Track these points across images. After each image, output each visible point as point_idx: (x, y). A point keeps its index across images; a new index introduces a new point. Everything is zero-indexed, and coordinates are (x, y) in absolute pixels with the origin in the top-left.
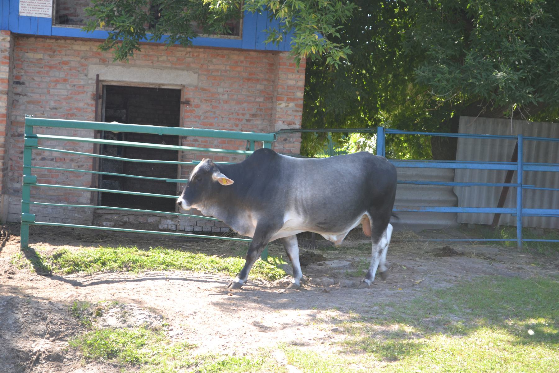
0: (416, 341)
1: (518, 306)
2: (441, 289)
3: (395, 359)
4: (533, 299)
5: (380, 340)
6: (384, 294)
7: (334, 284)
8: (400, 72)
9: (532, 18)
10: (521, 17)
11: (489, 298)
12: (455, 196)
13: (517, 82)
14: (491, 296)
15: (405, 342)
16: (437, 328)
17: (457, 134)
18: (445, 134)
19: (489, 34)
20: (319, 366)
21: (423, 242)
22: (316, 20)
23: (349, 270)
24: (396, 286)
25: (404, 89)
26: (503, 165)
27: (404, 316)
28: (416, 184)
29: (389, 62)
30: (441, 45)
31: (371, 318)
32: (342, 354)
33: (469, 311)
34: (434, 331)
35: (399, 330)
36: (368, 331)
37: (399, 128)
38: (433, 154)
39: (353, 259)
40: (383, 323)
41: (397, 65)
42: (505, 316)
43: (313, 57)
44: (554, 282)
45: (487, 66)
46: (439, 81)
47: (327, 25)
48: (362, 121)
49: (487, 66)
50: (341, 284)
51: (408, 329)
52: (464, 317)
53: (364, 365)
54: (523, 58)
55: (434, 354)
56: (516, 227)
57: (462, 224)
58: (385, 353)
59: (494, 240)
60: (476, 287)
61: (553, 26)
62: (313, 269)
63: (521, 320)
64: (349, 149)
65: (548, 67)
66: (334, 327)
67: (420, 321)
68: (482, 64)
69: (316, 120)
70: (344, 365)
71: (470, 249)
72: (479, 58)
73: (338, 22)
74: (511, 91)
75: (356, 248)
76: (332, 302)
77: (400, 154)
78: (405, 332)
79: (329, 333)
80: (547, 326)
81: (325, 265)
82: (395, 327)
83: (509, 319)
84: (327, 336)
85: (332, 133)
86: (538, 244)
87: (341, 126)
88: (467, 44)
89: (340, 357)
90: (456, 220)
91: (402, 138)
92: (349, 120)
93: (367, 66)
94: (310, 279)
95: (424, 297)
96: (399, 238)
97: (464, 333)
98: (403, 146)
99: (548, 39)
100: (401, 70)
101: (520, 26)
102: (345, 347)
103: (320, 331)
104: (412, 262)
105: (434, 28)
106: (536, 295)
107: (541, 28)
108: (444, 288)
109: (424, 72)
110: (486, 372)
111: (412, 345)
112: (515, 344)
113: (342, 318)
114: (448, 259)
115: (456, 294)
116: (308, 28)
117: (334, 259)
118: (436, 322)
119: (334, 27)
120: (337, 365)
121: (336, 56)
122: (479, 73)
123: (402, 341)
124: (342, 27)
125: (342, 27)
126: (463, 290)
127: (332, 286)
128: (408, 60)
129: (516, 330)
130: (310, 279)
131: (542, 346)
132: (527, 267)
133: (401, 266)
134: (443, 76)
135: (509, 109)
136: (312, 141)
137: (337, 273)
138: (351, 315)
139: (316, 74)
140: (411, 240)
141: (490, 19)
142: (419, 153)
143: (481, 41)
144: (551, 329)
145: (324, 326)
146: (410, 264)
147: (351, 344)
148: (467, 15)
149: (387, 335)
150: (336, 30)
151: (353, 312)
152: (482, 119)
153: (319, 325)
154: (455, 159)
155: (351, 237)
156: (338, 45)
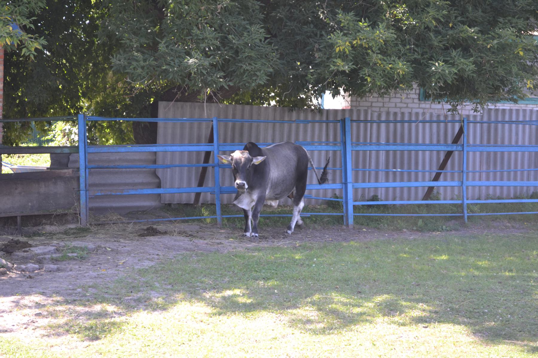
0: (117, 319)
1: (215, 279)
2: (144, 267)
3: (97, 338)
4: (230, 272)
5: (83, 322)
6: (88, 276)
7: (39, 269)
8: (99, 61)
9: (219, 6)
10: (209, 6)
11: (189, 274)
12: (158, 178)
13: (208, 68)
14: (191, 271)
15: (107, 321)
16: (138, 305)
17: (156, 119)
18: (144, 119)
19: (180, 23)
20: (21, 351)
21: (128, 223)
22: (10, 12)
23: (54, 255)
24: (100, 268)
25: (104, 78)
26: (200, 147)
27: (106, 296)
28: (120, 168)
29: (88, 51)
30: (134, 33)
31: (75, 301)
32: (45, 338)
33: (169, 287)
34: (136, 309)
35: (102, 310)
36: (71, 313)
37: (101, 114)
38: (135, 138)
39: (59, 244)
40: (85, 304)
41: (97, 54)
42: (202, 289)
43: (9, 48)
44: (250, 254)
45: (180, 53)
46: (134, 68)
47: (21, 16)
48: (64, 109)
49: (180, 53)
50: (46, 268)
51: (111, 308)
52: (164, 293)
53: (66, 346)
54: (213, 44)
55: (135, 331)
56: (215, 205)
57: (166, 204)
58: (87, 334)
59: (196, 218)
60: (176, 264)
61: (239, 14)
62: (18, 256)
63: (218, 292)
64: (55, 137)
65: (237, 52)
66: (37, 311)
67: (122, 300)
68: (175, 51)
69: (18, 110)
70: (47, 348)
71: (172, 228)
72: (172, 45)
73: (31, 14)
74: (203, 77)
75: (62, 233)
76: (36, 287)
77: (104, 139)
78: (107, 311)
79: (33, 318)
80: (242, 296)
81: (30, 251)
82: (97, 308)
83: (206, 292)
84: (30, 321)
85: (35, 122)
86: (236, 220)
87: (44, 115)
88: (161, 35)
89: (42, 340)
90: (160, 201)
91: (105, 125)
92: (51, 108)
93: (66, 55)
94: (15, 266)
95: (126, 276)
96: (105, 221)
97: (164, 308)
98: (106, 132)
99: (235, 26)
100: (100, 59)
101: (209, 14)
102: (49, 331)
103: (24, 317)
104: (116, 244)
105: (128, 17)
106: (233, 268)
107: (229, 16)
108: (147, 266)
109: (120, 61)
110: (184, 344)
111: (114, 324)
112: (212, 315)
113: (46, 303)
114: (152, 238)
115: (157, 271)
116: (2, 20)
117: (40, 245)
118: (137, 300)
119: (28, 18)
120: (39, 348)
121: (32, 47)
122: (172, 60)
123: (104, 320)
124: (36, 18)
125: (36, 18)
126: (164, 267)
127: (36, 272)
128: (106, 49)
129: (213, 301)
130: (15, 266)
131: (237, 314)
132: (225, 242)
133: (105, 248)
134: (137, 63)
135: (203, 93)
136: (16, 130)
137: (43, 258)
138: (54, 299)
139: (17, 65)
140: (116, 222)
141: (180, 9)
142: (121, 138)
143: (173, 29)
144: (245, 299)
145: (27, 311)
146: (115, 246)
147: (54, 327)
148: (159, 5)
149: (89, 316)
150: (30, 21)
151: (56, 296)
152: (179, 104)
153: (22, 311)
154: (156, 143)
155: (56, 223)
156: (32, 36)
